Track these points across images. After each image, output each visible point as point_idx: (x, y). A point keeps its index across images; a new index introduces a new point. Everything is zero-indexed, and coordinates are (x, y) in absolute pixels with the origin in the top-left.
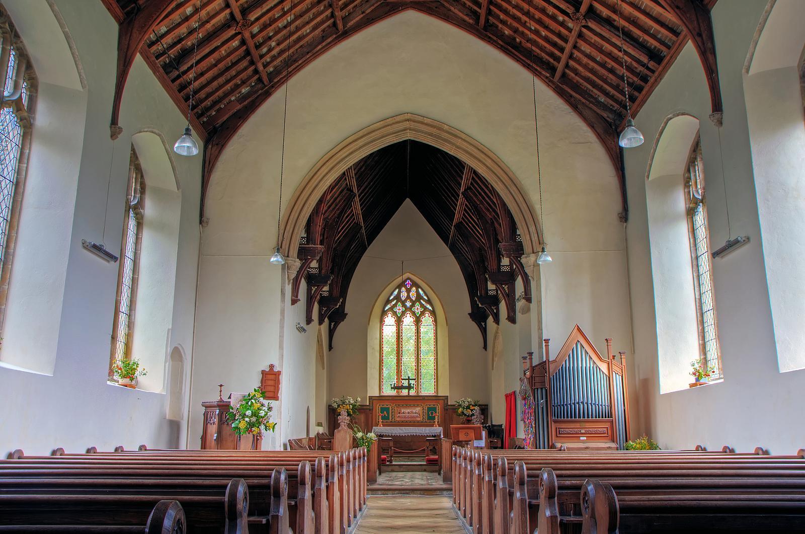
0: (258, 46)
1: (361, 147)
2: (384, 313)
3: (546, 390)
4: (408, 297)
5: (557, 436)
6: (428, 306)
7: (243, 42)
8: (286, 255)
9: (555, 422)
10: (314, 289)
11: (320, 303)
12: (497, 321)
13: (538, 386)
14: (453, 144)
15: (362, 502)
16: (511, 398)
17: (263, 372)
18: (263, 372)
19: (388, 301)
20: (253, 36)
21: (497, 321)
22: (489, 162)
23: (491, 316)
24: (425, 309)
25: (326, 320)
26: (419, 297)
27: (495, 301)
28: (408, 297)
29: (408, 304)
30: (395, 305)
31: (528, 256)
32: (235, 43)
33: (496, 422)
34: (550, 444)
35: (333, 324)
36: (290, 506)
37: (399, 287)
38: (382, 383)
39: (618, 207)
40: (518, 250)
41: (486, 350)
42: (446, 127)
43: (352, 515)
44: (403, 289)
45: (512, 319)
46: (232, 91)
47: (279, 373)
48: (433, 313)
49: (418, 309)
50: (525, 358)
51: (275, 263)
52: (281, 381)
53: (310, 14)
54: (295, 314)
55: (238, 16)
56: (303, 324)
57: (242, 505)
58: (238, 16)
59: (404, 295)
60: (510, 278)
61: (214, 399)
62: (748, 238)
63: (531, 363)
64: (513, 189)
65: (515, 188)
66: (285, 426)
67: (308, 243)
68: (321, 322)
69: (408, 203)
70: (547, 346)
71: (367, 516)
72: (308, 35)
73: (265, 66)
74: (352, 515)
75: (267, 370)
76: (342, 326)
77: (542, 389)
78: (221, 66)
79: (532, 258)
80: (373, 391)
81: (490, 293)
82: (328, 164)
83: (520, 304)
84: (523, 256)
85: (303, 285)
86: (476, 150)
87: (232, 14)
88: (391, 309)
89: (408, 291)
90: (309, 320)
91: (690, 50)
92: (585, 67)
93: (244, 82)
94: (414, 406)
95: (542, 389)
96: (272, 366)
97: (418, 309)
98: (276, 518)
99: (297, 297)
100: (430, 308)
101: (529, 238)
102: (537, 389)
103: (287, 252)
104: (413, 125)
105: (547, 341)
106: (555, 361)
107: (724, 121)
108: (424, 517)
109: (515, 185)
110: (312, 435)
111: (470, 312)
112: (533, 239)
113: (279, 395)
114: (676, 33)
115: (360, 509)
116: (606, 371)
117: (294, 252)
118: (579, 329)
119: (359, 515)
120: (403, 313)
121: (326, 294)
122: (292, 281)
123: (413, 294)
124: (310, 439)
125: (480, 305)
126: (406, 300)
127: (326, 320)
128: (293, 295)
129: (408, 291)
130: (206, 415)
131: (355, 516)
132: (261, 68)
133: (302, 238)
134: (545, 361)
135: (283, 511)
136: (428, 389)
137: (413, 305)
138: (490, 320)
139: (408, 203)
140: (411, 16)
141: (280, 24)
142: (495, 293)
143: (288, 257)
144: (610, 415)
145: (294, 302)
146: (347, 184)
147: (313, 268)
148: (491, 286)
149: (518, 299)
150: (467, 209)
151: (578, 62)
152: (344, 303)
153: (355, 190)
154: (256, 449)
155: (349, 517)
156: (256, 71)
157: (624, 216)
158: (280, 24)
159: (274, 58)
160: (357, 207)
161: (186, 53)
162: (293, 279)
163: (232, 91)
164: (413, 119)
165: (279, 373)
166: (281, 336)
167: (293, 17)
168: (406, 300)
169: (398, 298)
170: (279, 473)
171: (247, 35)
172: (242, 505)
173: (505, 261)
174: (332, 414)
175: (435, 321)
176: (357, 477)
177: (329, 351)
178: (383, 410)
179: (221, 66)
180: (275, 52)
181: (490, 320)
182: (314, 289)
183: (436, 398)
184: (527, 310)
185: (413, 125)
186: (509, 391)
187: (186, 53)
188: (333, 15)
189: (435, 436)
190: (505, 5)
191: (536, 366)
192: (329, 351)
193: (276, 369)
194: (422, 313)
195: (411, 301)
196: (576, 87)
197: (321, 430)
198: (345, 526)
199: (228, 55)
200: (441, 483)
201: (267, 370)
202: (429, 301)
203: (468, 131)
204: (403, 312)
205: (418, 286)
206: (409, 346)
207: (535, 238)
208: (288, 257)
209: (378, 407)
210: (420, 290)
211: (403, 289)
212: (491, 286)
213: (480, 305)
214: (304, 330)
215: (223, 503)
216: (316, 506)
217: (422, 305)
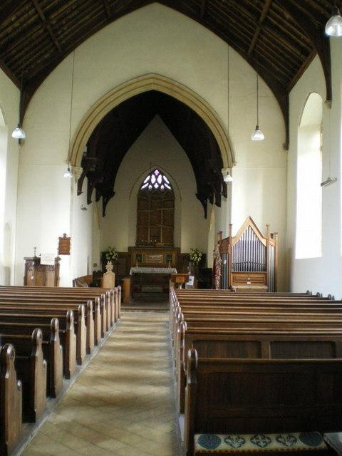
0: (55, 31)
1: (122, 95)
4: (156, 182)
7: (46, 30)
12: (212, 202)
14: (181, 95)
15: (117, 317)
17: (60, 238)
18: (60, 238)
20: (52, 26)
25: (101, 198)
28: (156, 182)
32: (41, 31)
36: (75, 324)
37: (151, 175)
39: (283, 140)
43: (109, 325)
46: (39, 58)
47: (69, 239)
53: (90, 9)
55: (43, 18)
56: (86, 205)
57: (57, 327)
58: (43, 18)
59: (153, 180)
61: (31, 256)
62: (336, 179)
63: (221, 238)
64: (218, 127)
66: (71, 271)
67: (88, 156)
68: (97, 200)
70: (230, 228)
71: (122, 320)
72: (88, 20)
73: (60, 41)
74: (109, 325)
75: (62, 236)
78: (33, 45)
79: (228, 170)
87: (40, 18)
89: (157, 177)
90: (89, 202)
91: (316, 63)
92: (266, 49)
93: (46, 52)
94: (158, 254)
96: (65, 235)
98: (69, 331)
104: (155, 81)
107: (332, 106)
108: (152, 326)
111: (196, 192)
114: (312, 48)
115: (115, 322)
116: (265, 244)
117: (79, 162)
118: (251, 219)
119: (114, 324)
126: (154, 184)
127: (101, 198)
128: (78, 189)
129: (157, 177)
130: (26, 265)
131: (111, 325)
132: (57, 43)
135: (72, 328)
138: (208, 201)
140: (157, 8)
141: (70, 17)
144: (265, 269)
151: (262, 45)
155: (107, 326)
156: (54, 45)
157: (286, 146)
158: (70, 17)
159: (67, 35)
161: (12, 41)
163: (39, 58)
164: (156, 77)
165: (69, 239)
167: (78, 11)
170: (70, 313)
171: (48, 27)
172: (57, 327)
174: (104, 258)
176: (113, 304)
178: (138, 256)
179: (33, 45)
180: (66, 33)
185: (155, 81)
187: (12, 41)
188: (104, 7)
190: (219, 3)
193: (68, 236)
195: (158, 184)
196: (261, 60)
198: (105, 331)
199: (37, 38)
201: (62, 236)
203: (191, 87)
205: (163, 175)
211: (153, 176)
215: (50, 327)
216: (87, 323)
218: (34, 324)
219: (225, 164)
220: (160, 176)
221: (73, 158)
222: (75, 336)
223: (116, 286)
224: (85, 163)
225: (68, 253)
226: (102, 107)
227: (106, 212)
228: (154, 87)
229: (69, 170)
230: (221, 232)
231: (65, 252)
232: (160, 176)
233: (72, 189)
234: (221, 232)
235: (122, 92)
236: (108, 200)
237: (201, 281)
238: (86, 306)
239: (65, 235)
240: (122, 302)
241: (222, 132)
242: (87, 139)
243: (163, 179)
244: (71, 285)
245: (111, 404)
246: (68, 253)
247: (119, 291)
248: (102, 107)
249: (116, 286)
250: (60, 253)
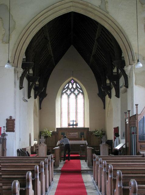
2: (62, 94)
3: (136, 128)
4: (72, 87)
5: (140, 148)
6: (81, 91)
8: (16, 66)
9: (140, 142)
10: (31, 83)
11: (35, 90)
12: (110, 97)
13: (132, 126)
16: (116, 130)
17: (7, 120)
18: (7, 120)
19: (64, 89)
21: (110, 97)
22: (110, 22)
23: (107, 95)
24: (80, 92)
25: (38, 97)
26: (77, 87)
27: (110, 89)
28: (72, 87)
29: (72, 90)
30: (67, 91)
31: (128, 66)
33: (109, 139)
34: (137, 152)
35: (41, 98)
37: (69, 83)
38: (62, 121)
40: (122, 64)
41: (105, 109)
42: (90, 5)
44: (70, 84)
45: (118, 95)
47: (14, 120)
48: (83, 93)
49: (76, 92)
50: (126, 113)
51: (7, 68)
52: (15, 123)
54: (22, 94)
56: (26, 98)
59: (70, 86)
60: (117, 78)
63: (129, 115)
64: (121, 35)
65: (122, 34)
67: (27, 61)
68: (35, 98)
69: (72, 46)
70: (137, 108)
75: (9, 119)
76: (45, 99)
77: (134, 127)
79: (130, 67)
80: (58, 126)
81: (107, 85)
82: (34, 23)
83: (121, 90)
84: (125, 66)
85: (25, 81)
86: (103, 16)
88: (65, 92)
89: (72, 85)
90: (29, 97)
95: (134, 127)
96: (11, 117)
97: (76, 92)
99: (22, 86)
100: (81, 91)
101: (128, 58)
102: (132, 127)
103: (16, 65)
105: (137, 105)
106: (140, 114)
109: (122, 32)
110: (32, 145)
111: (98, 93)
112: (130, 59)
113: (15, 130)
120: (70, 94)
121: (37, 86)
122: (19, 78)
123: (74, 86)
124: (32, 147)
125: (103, 90)
126: (71, 89)
127: (38, 97)
129: (72, 85)
133: (24, 59)
134: (136, 114)
136: (81, 125)
137: (74, 91)
138: (107, 96)
139: (72, 46)
142: (109, 85)
143: (17, 67)
145: (21, 88)
146: (44, 36)
147: (31, 74)
148: (108, 82)
149: (121, 87)
150: (98, 48)
152: (45, 89)
153: (48, 38)
154: (4, 156)
160: (50, 48)
162: (20, 77)
165: (14, 120)
166: (15, 103)
168: (71, 89)
169: (68, 88)
173: (115, 70)
175: (84, 97)
177: (40, 109)
181: (107, 96)
182: (31, 83)
183: (84, 129)
184: (126, 91)
186: (116, 126)
189: (83, 145)
191: (132, 117)
192: (40, 109)
193: (13, 118)
194: (78, 94)
195: (74, 88)
197: (36, 142)
200: (87, 166)
201: (9, 119)
202: (81, 89)
204: (70, 93)
205: (76, 83)
206: (72, 109)
207: (131, 58)
208: (17, 67)
209: (60, 133)
210: (77, 84)
211: (70, 84)
212: (108, 82)
213: (103, 90)
214: (27, 101)
217: (78, 91)
218: (28, 169)
219: (127, 62)
220: (75, 84)
221: (16, 62)
222: (48, 171)
223: (48, 153)
224: (25, 66)
225: (13, 131)
226: (35, 23)
227: (41, 107)
228: (72, 10)
229: (9, 62)
230: (129, 111)
231: (11, 130)
232: (75, 84)
233: (15, 83)
234: (129, 111)
235: (50, 13)
236: (43, 99)
237: (60, 161)
238: (39, 166)
239: (11, 117)
240: (54, 166)
241: (124, 40)
242: (26, 48)
243: (76, 85)
244: (15, 154)
245: (76, 104)
246: (13, 131)
247: (52, 159)
248: (35, 23)
249: (48, 153)
250: (7, 131)
